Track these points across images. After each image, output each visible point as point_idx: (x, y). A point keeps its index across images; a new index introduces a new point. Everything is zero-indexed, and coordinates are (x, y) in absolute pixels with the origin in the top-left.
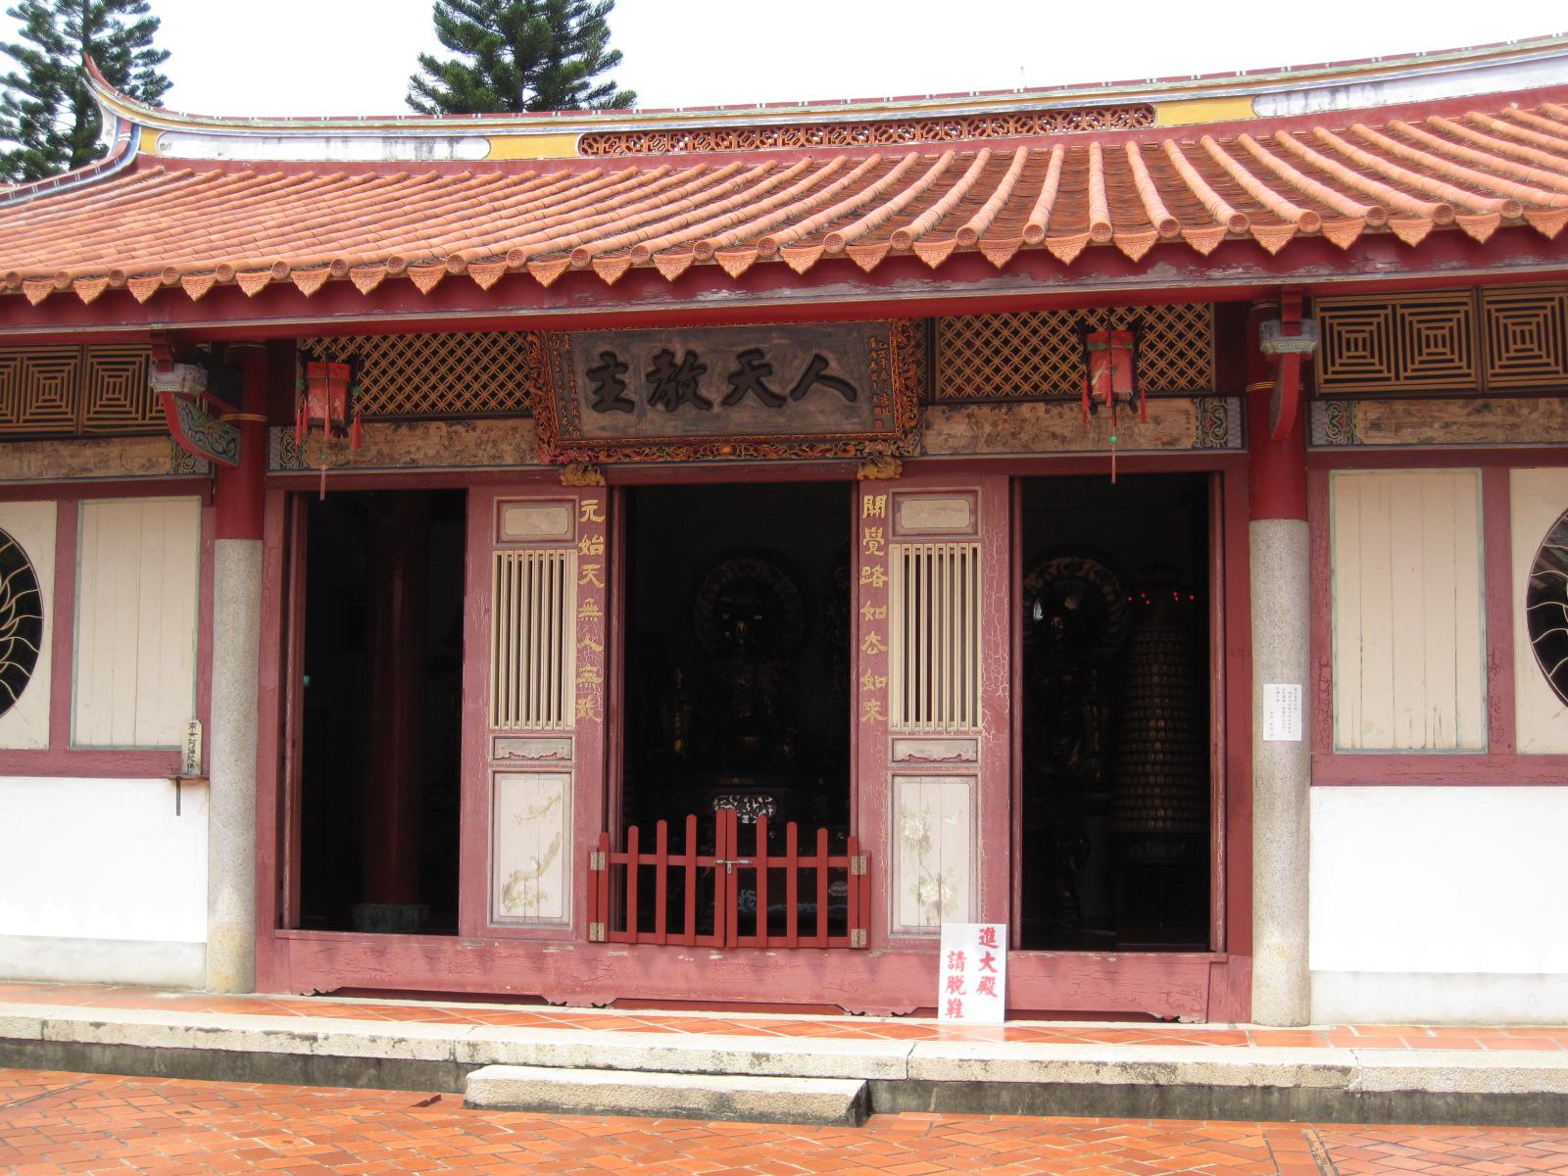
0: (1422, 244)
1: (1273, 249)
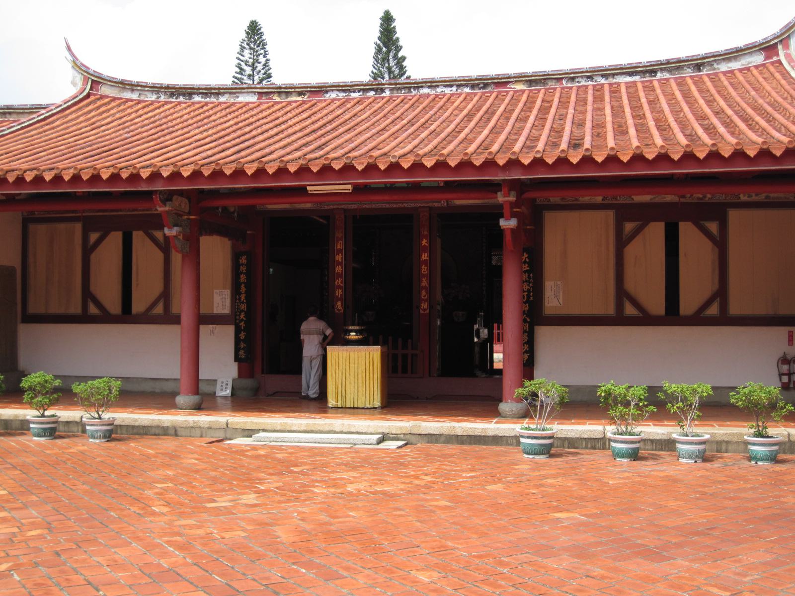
0: (654, 159)
1: (575, 162)
